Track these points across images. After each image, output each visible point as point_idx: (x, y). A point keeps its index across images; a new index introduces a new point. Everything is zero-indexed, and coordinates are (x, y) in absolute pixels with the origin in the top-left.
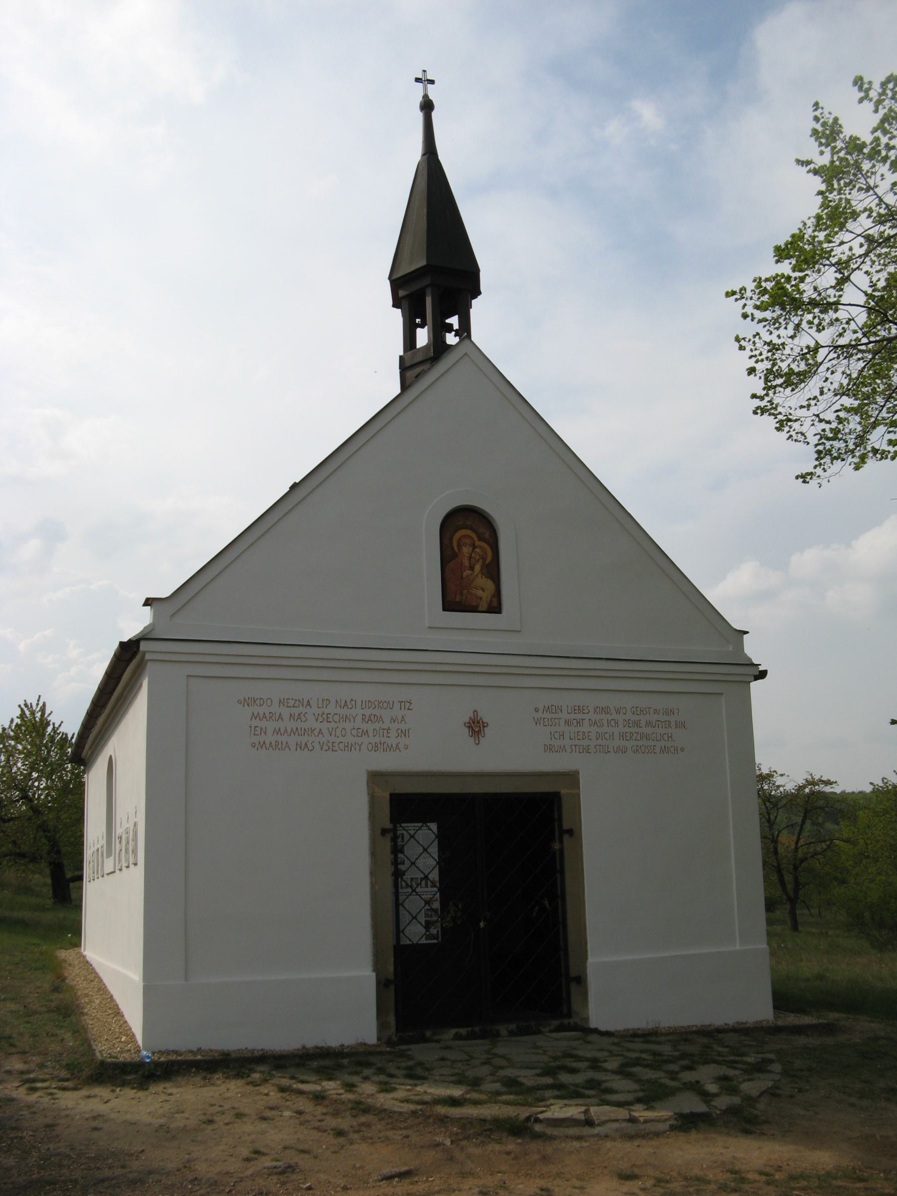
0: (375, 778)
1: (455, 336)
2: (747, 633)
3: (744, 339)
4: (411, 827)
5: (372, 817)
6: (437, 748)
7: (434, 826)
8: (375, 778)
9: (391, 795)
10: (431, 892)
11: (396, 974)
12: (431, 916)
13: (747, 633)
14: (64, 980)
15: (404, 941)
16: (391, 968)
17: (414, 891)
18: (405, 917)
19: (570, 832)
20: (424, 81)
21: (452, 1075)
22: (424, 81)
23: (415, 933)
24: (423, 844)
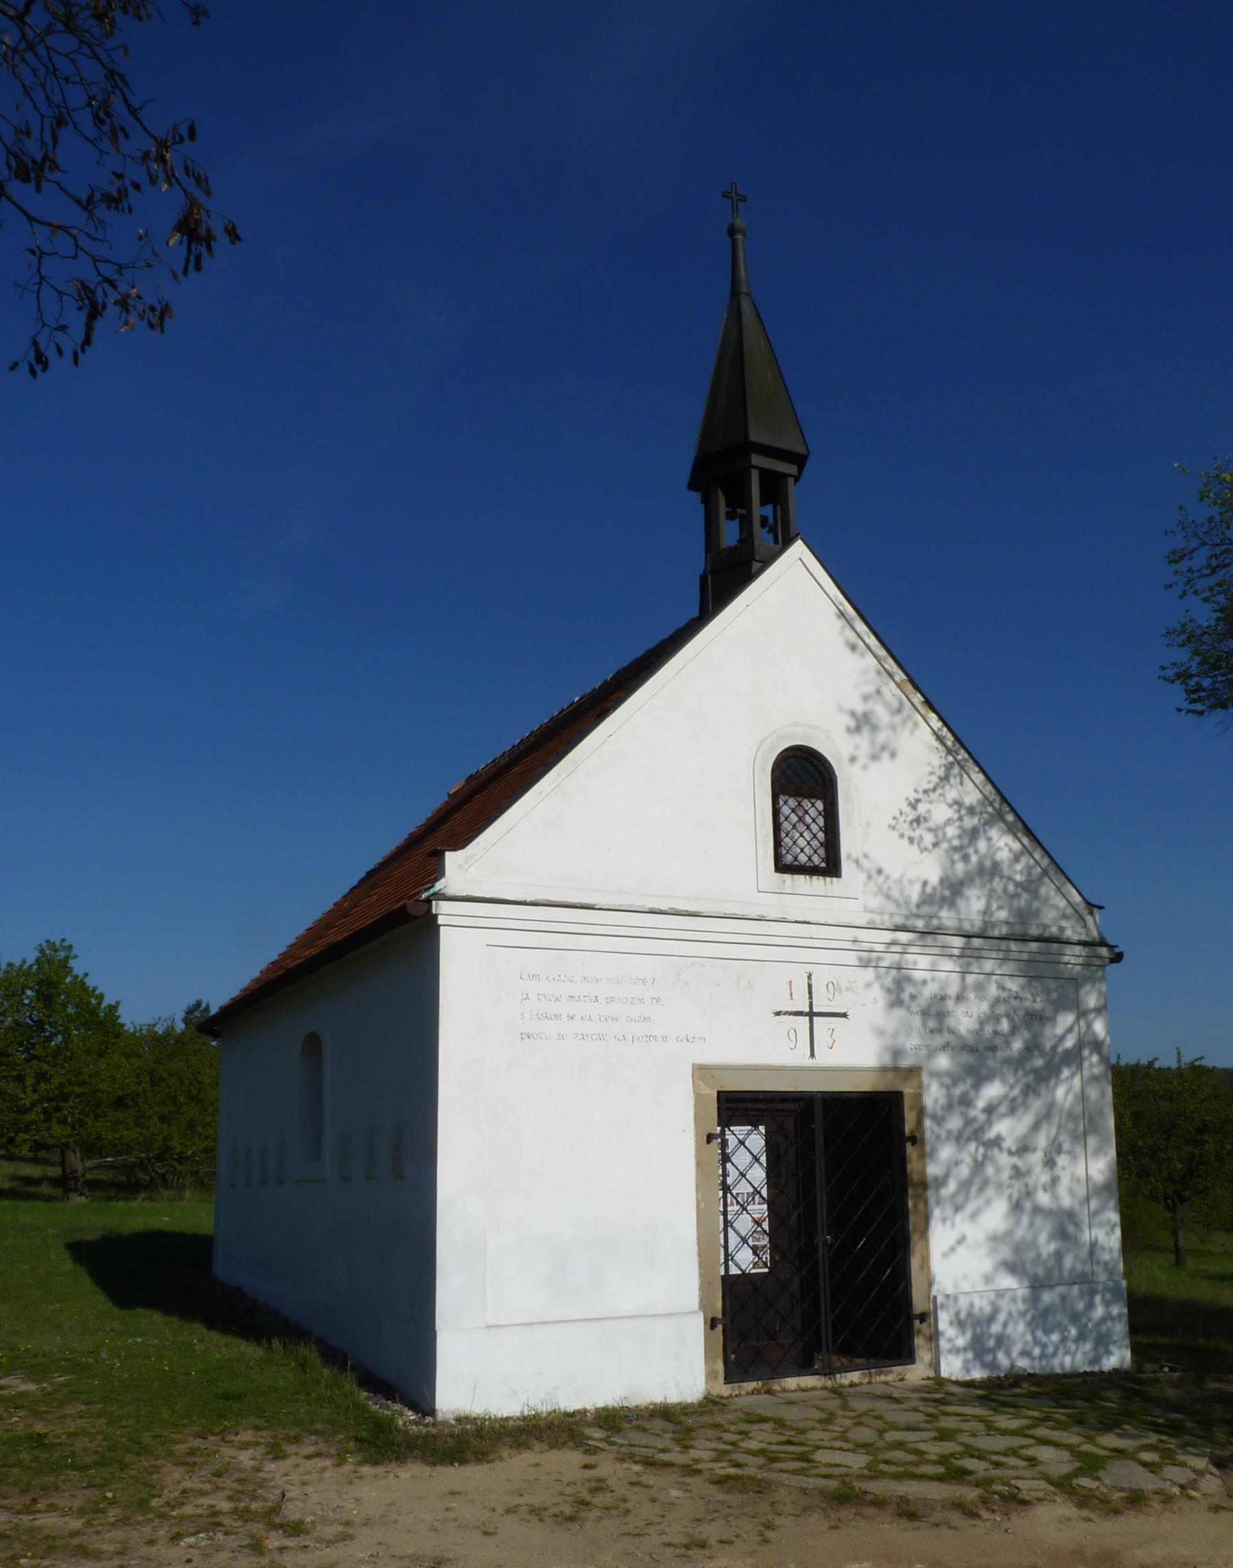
0: (702, 1072)
1: (769, 532)
2: (163, 332)
3: (902, 836)
4: (740, 1130)
5: (698, 1119)
6: (775, 1052)
7: (762, 1129)
8: (702, 1072)
9: (719, 1093)
10: (760, 1209)
11: (724, 1313)
12: (759, 1240)
13: (163, 332)
14: (28, 973)
15: (734, 1271)
16: (719, 1304)
17: (745, 1209)
18: (733, 1240)
19: (923, 1317)
20: (734, 198)
21: (777, 1444)
22: (734, 198)
23: (745, 1260)
24: (750, 1142)
